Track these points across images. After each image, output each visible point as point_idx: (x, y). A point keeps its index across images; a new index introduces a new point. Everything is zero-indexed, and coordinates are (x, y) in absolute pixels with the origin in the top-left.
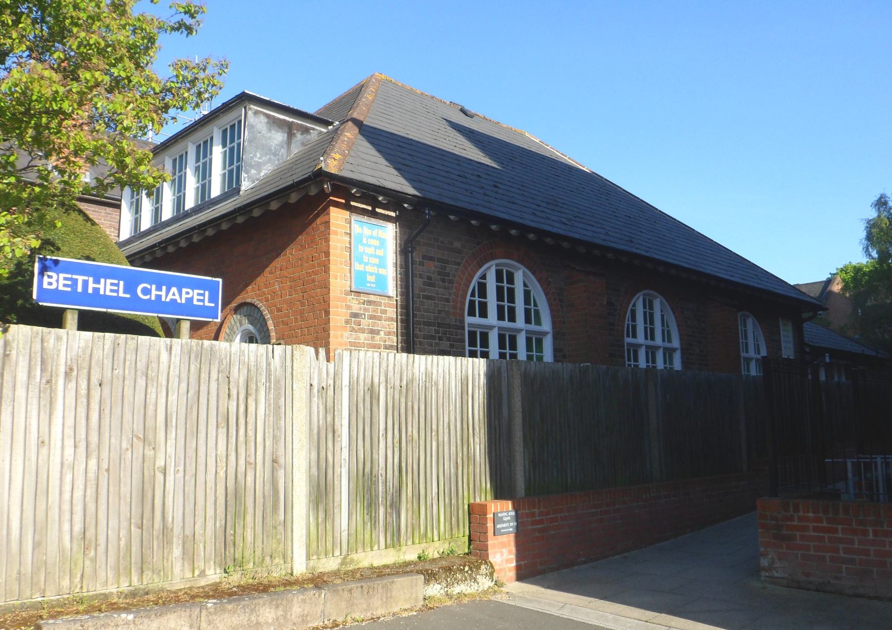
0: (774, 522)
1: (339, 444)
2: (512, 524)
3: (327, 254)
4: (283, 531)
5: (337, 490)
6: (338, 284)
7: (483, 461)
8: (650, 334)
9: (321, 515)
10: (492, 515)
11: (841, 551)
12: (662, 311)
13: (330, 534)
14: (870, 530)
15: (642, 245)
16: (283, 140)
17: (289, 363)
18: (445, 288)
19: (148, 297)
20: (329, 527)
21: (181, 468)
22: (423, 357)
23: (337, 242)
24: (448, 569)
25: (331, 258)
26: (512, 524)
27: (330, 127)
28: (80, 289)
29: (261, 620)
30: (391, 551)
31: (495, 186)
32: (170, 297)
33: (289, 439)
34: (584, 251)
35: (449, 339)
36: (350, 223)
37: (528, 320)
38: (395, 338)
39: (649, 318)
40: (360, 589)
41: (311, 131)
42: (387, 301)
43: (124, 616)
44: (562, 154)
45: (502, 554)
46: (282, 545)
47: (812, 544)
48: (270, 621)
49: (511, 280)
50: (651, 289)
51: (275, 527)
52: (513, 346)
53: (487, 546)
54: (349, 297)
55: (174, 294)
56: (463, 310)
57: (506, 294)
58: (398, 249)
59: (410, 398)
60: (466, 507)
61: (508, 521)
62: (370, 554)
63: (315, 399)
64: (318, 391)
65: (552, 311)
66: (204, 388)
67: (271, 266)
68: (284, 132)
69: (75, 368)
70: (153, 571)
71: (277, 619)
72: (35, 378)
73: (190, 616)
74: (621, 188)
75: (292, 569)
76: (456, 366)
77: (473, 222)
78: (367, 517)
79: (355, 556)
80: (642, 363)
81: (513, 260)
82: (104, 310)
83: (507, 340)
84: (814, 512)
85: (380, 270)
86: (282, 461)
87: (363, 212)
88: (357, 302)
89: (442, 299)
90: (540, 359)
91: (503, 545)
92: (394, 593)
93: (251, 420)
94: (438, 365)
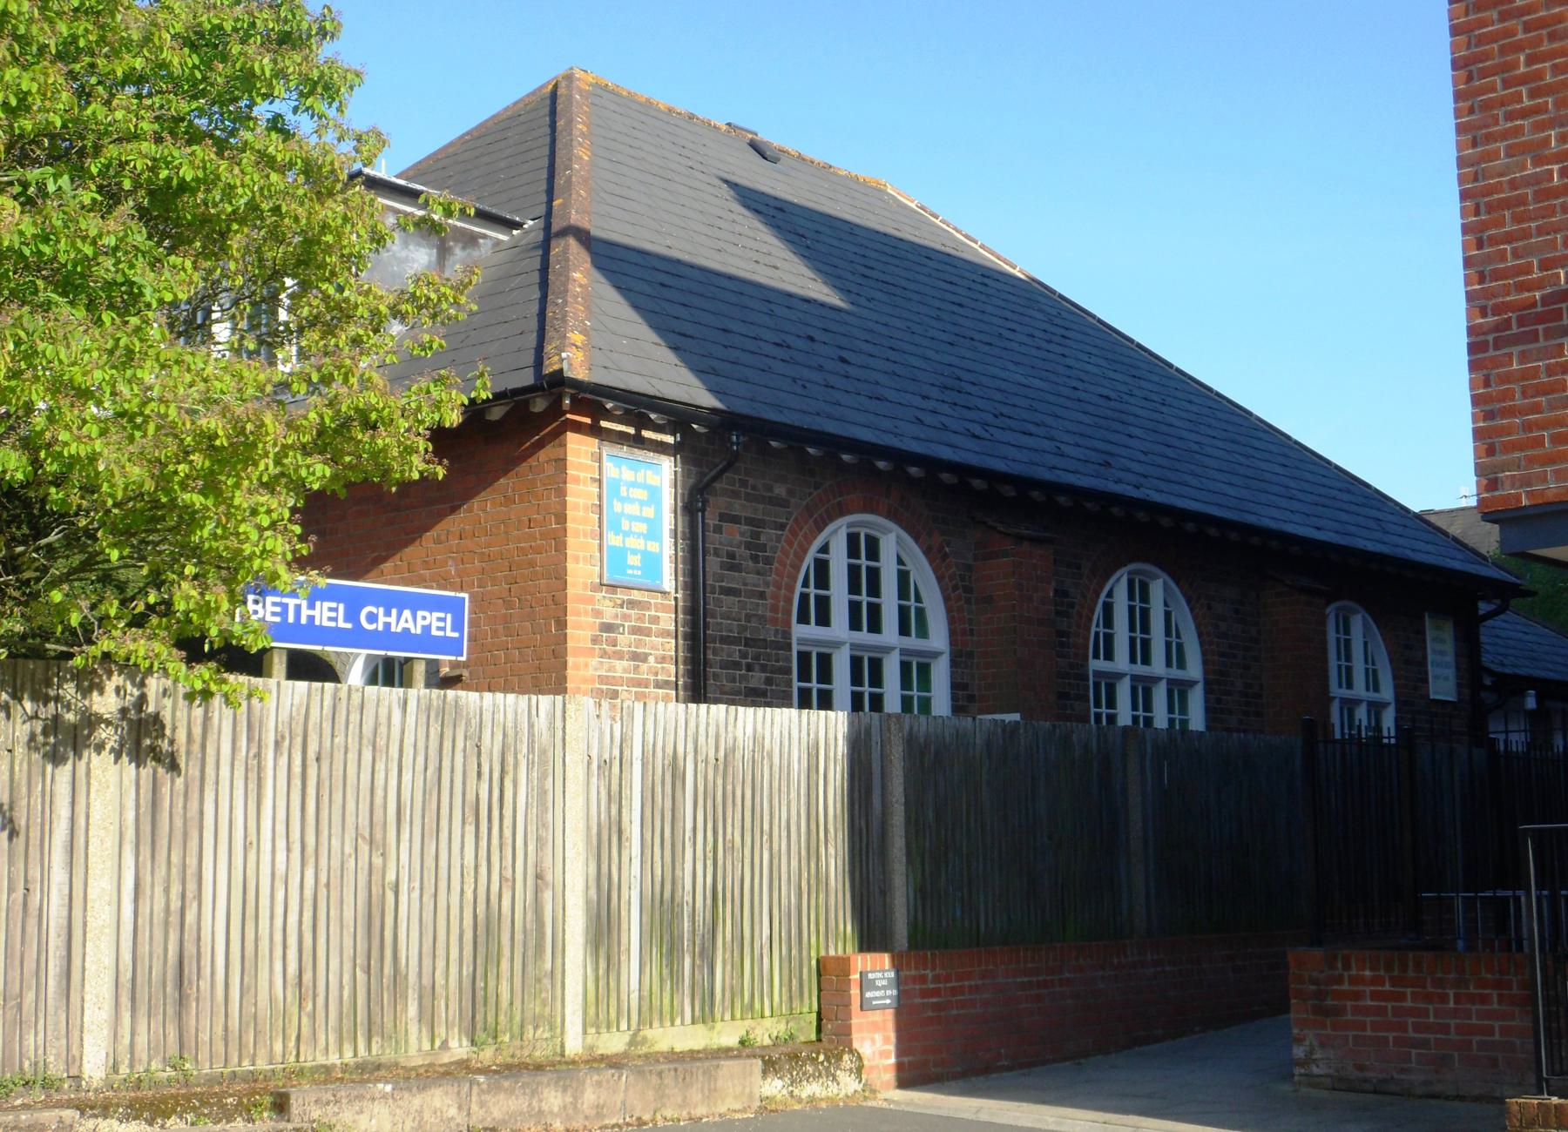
0: (1313, 987)
1: (627, 851)
2: (889, 992)
3: (562, 518)
4: (549, 987)
5: (624, 926)
6: (580, 571)
7: (840, 887)
8: (1140, 651)
9: (603, 965)
10: (858, 976)
11: (1410, 1029)
12: (1166, 605)
13: (614, 995)
14: (1451, 993)
15: (1129, 470)
16: (430, 262)
17: (559, 724)
18: (758, 573)
19: (372, 627)
20: (613, 984)
21: (417, 885)
22: (751, 710)
23: (579, 495)
24: (794, 1057)
25: (569, 525)
26: (889, 992)
27: (515, 232)
28: (291, 619)
29: (545, 1107)
30: (700, 1027)
31: (843, 360)
32: (402, 624)
33: (559, 842)
34: (1013, 494)
35: (764, 669)
36: (600, 460)
37: (904, 630)
38: (673, 668)
39: (1140, 620)
40: (672, 1073)
41: (481, 241)
42: (659, 599)
43: (380, 1086)
44: (966, 236)
45: (873, 1042)
46: (548, 1009)
47: (1368, 1019)
48: (556, 1109)
49: (873, 554)
50: (1146, 560)
51: (538, 980)
52: (876, 680)
53: (850, 1027)
54: (599, 595)
55: (407, 621)
56: (789, 612)
57: (864, 580)
58: (680, 504)
59: (730, 780)
60: (814, 962)
61: (884, 988)
62: (678, 1028)
63: (594, 780)
64: (599, 767)
65: (949, 610)
66: (446, 763)
67: (438, 527)
68: (430, 246)
69: (287, 735)
70: (383, 1037)
71: (565, 1108)
72: (240, 750)
73: (459, 1093)
74: (1093, 316)
75: (563, 1046)
76: (800, 726)
77: (811, 450)
78: (666, 972)
79: (647, 1032)
80: (1124, 716)
81: (880, 515)
82: (319, 648)
83: (867, 669)
84: (1372, 969)
85: (649, 543)
86: (549, 877)
87: (621, 438)
88: (611, 604)
89: (752, 594)
90: (925, 705)
91: (875, 1027)
92: (720, 1083)
93: (508, 812)
94: (772, 723)
